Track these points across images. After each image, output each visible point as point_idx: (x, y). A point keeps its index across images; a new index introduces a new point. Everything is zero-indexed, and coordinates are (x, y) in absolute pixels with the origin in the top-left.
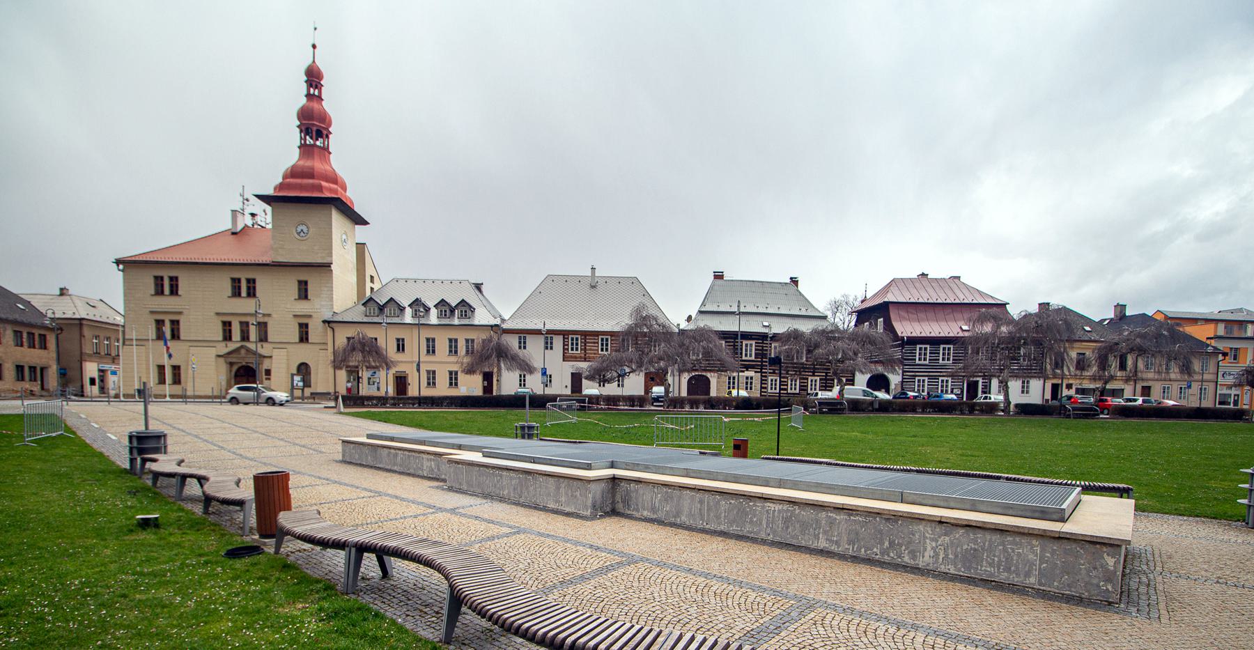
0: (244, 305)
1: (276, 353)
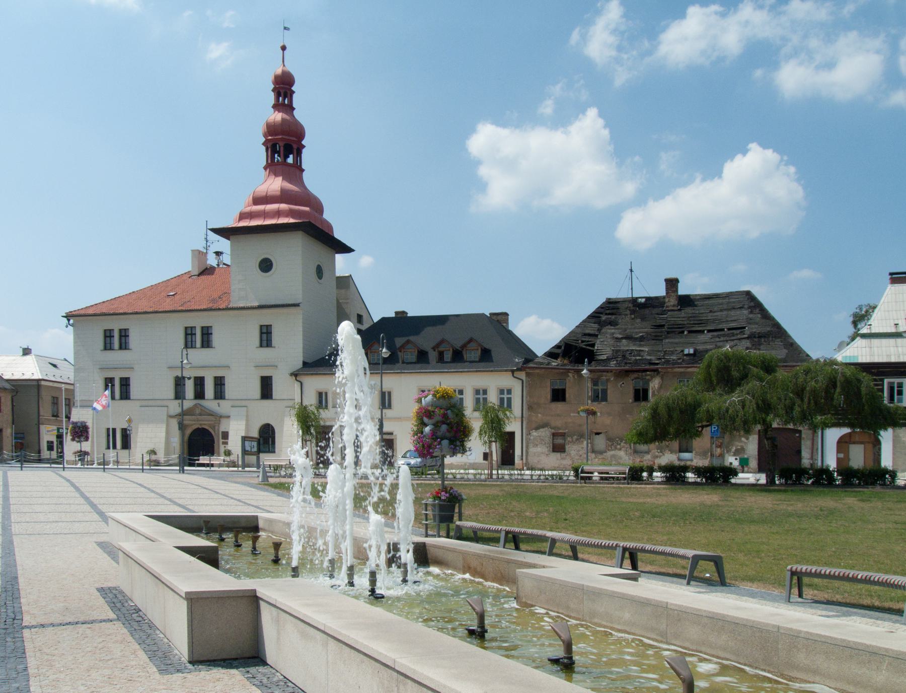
0: (198, 356)
1: (233, 412)
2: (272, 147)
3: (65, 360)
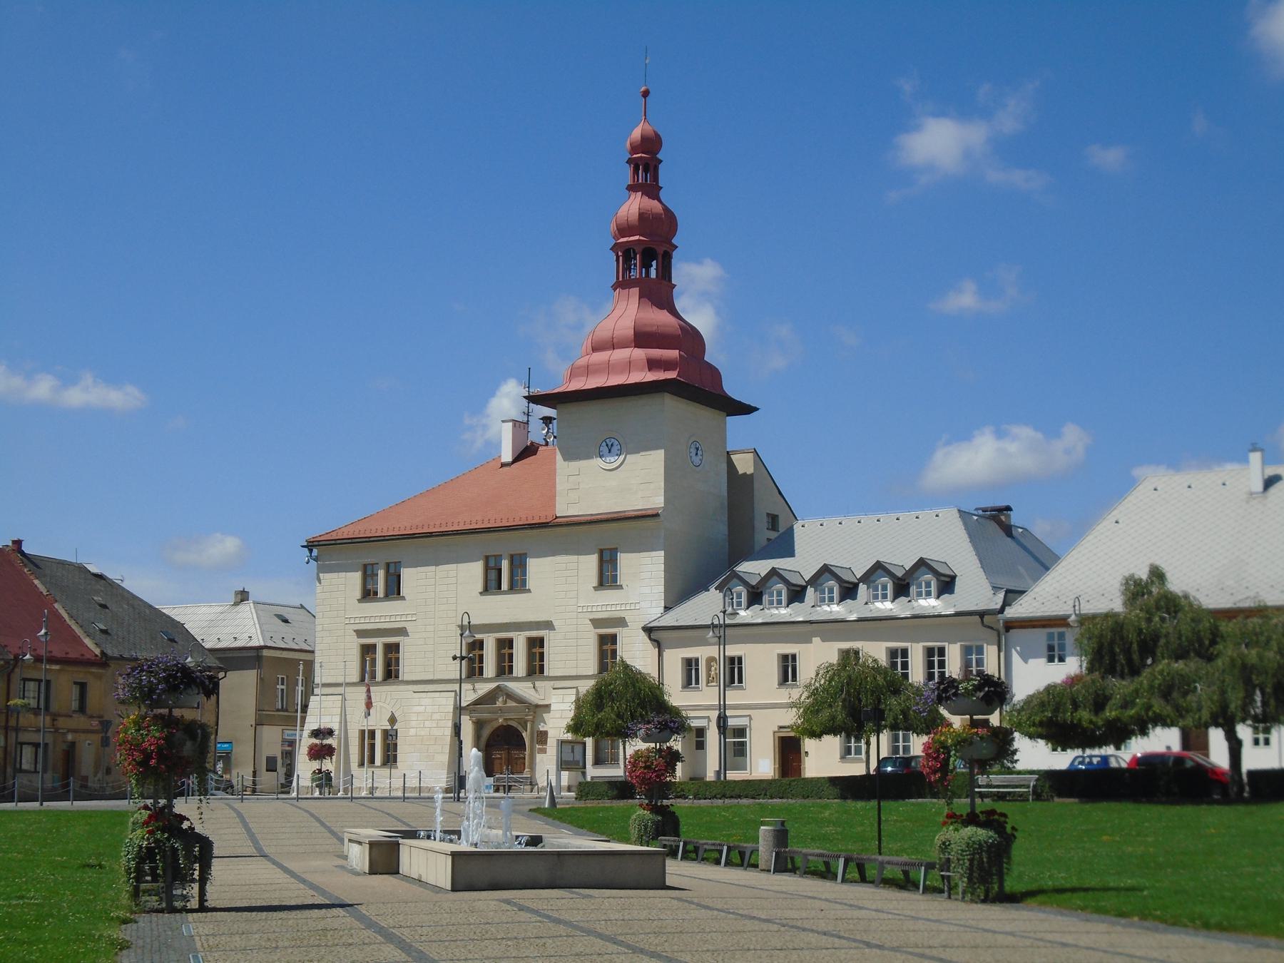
0: (504, 608)
2: (626, 254)
3: (302, 607)
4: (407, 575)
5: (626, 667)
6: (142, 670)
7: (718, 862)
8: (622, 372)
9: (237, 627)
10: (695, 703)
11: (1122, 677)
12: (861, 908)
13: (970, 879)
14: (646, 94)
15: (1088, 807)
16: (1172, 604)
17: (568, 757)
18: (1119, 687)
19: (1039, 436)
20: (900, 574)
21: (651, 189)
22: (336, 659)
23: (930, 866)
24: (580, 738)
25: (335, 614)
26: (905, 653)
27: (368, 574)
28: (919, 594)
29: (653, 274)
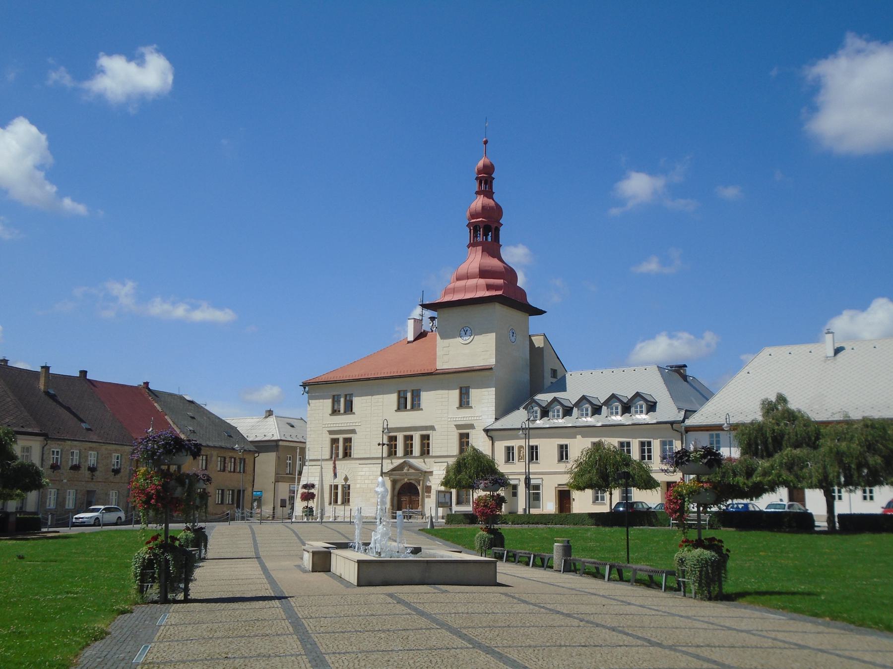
0: (409, 419)
2: (475, 229)
4: (357, 401)
5: (474, 449)
6: (150, 440)
7: (527, 564)
8: (472, 291)
9: (270, 430)
10: (514, 471)
11: (762, 458)
12: (629, 604)
13: (700, 585)
14: (486, 142)
15: (743, 533)
16: (792, 416)
17: (442, 500)
18: (763, 464)
19: (692, 337)
20: (625, 401)
21: (488, 193)
22: (318, 446)
23: (671, 573)
24: (448, 489)
25: (318, 421)
26: (628, 444)
27: (335, 400)
28: (636, 412)
29: (489, 239)
